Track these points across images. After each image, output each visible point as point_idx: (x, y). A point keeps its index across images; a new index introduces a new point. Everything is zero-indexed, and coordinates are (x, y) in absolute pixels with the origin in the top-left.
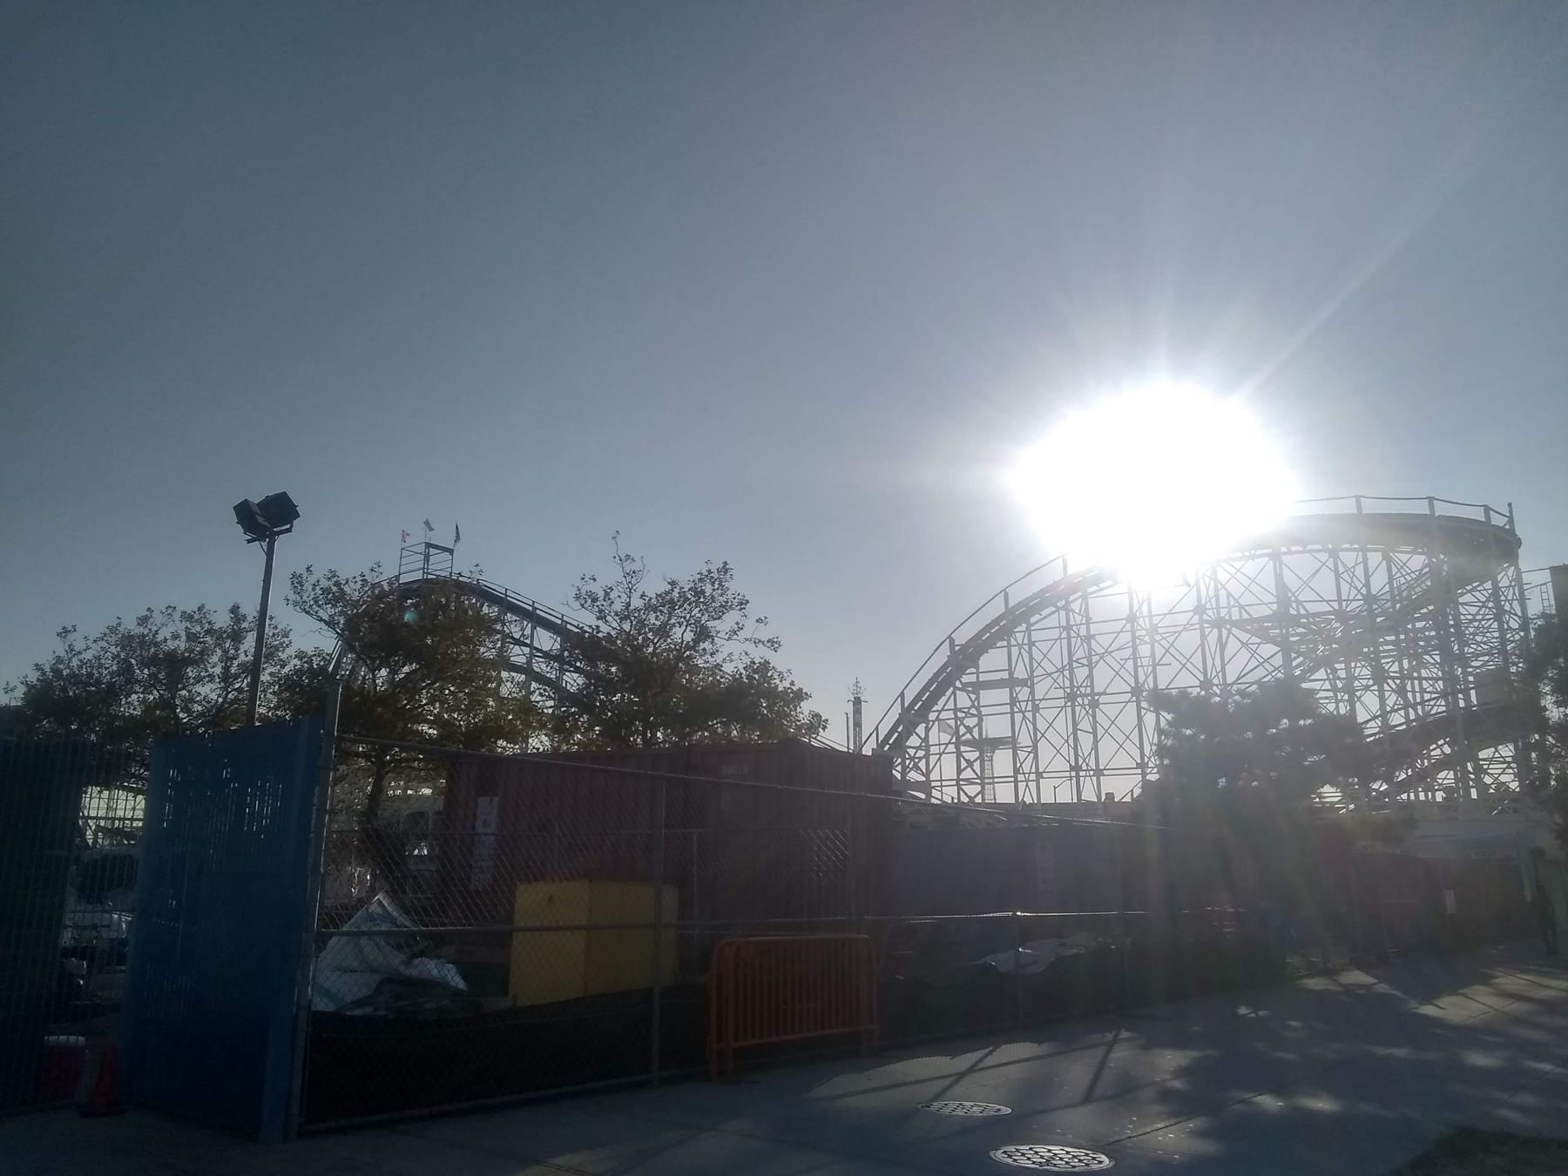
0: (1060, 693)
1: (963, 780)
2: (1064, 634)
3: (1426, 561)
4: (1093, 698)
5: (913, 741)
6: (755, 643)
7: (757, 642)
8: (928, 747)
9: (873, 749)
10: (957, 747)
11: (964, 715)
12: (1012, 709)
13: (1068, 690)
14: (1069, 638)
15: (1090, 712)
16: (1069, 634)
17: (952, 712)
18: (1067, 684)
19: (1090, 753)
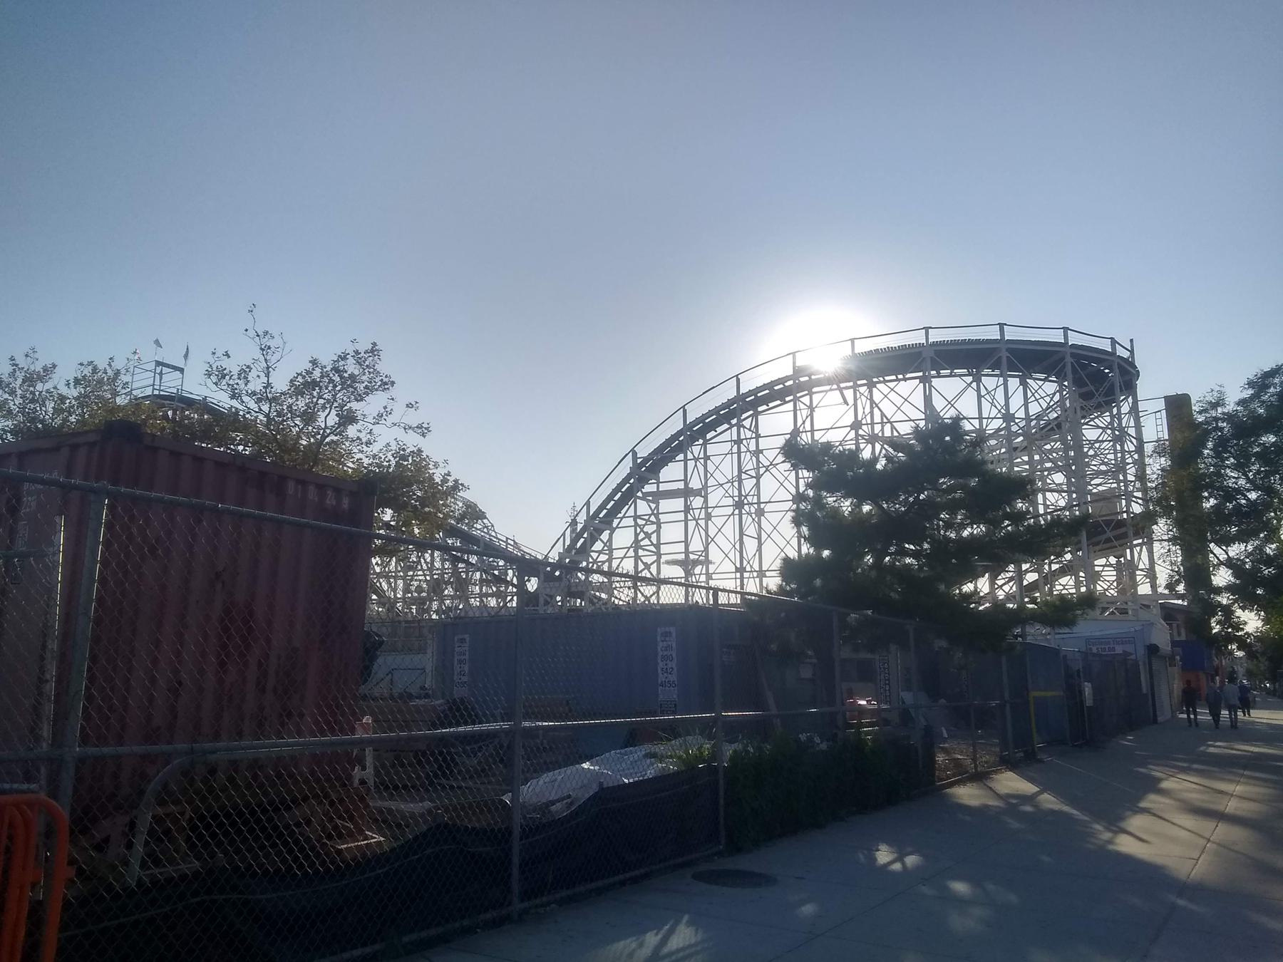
0: (730, 501)
2: (735, 449)
3: (1058, 389)
4: (759, 506)
5: (598, 546)
6: (405, 429)
7: (407, 428)
8: (611, 550)
10: (636, 552)
11: (644, 522)
12: (686, 517)
13: (737, 499)
14: (739, 453)
15: (756, 519)
16: (739, 448)
17: (632, 518)
18: (736, 493)
19: (755, 555)
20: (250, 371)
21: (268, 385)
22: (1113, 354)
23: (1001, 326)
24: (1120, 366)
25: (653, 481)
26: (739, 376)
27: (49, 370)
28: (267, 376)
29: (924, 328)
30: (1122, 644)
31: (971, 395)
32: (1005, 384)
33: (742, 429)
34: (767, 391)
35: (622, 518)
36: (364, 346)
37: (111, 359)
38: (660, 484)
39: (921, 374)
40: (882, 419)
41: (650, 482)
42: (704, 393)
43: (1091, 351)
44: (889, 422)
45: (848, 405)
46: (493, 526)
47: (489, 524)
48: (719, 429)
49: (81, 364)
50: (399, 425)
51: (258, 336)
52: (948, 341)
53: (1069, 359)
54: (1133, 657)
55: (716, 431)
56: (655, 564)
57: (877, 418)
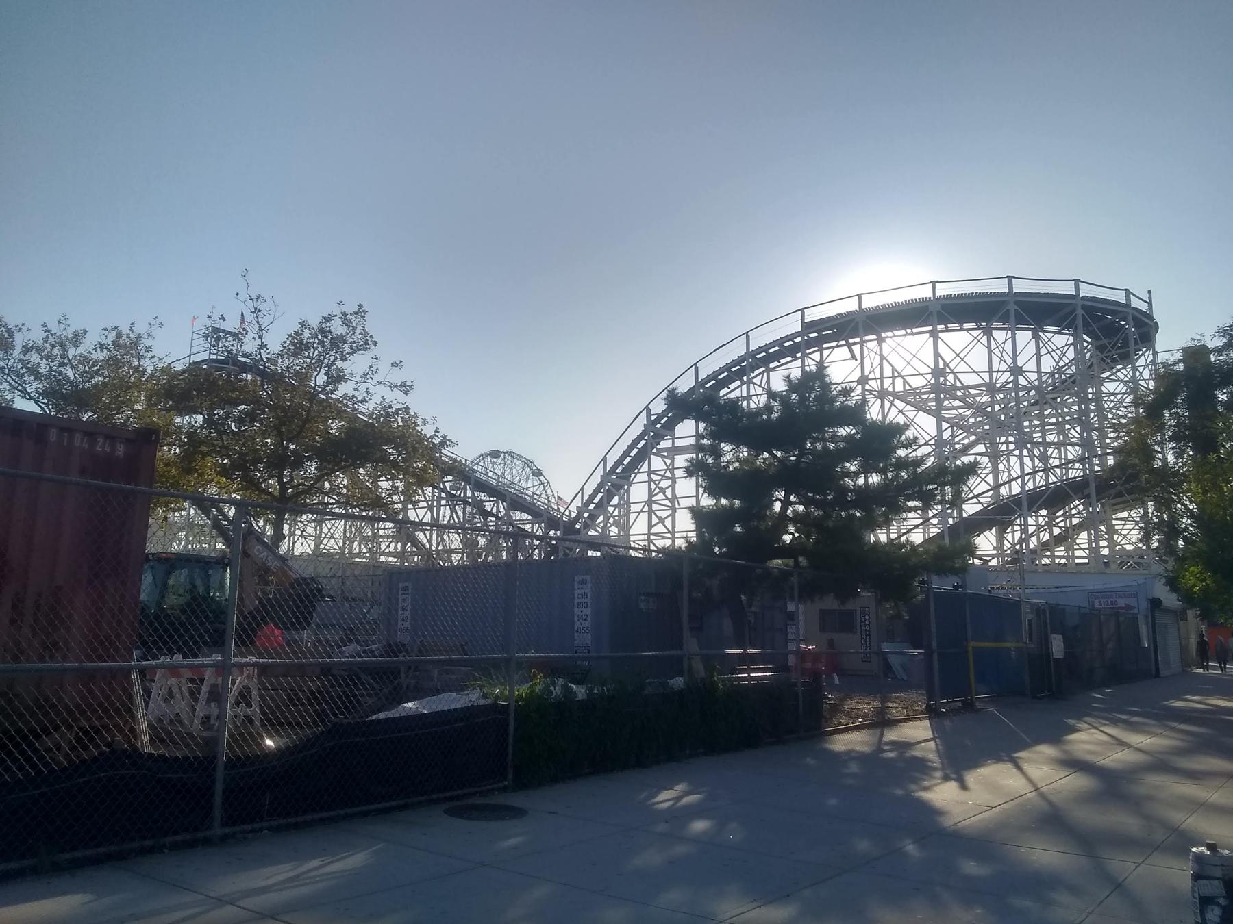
1: (654, 534)
6: (391, 387)
9: (577, 507)
10: (650, 507)
11: (659, 478)
17: (646, 474)
20: (246, 334)
21: (263, 346)
22: (1128, 305)
23: (1010, 278)
24: (1134, 318)
25: (669, 437)
26: (749, 333)
27: (77, 339)
28: (261, 337)
29: (931, 282)
30: (1125, 597)
31: (981, 351)
32: (1013, 338)
33: (751, 385)
34: (777, 348)
35: (636, 474)
36: (351, 308)
37: (132, 324)
38: (676, 440)
39: (931, 328)
40: (893, 373)
41: (666, 438)
42: (715, 351)
43: (1061, 298)
44: (900, 376)
45: (856, 360)
46: (548, 483)
47: (546, 481)
48: (732, 386)
49: (105, 330)
50: (384, 384)
51: (251, 299)
52: (955, 295)
53: (1080, 312)
54: (1135, 611)
55: (729, 388)
56: (670, 518)
57: (888, 372)
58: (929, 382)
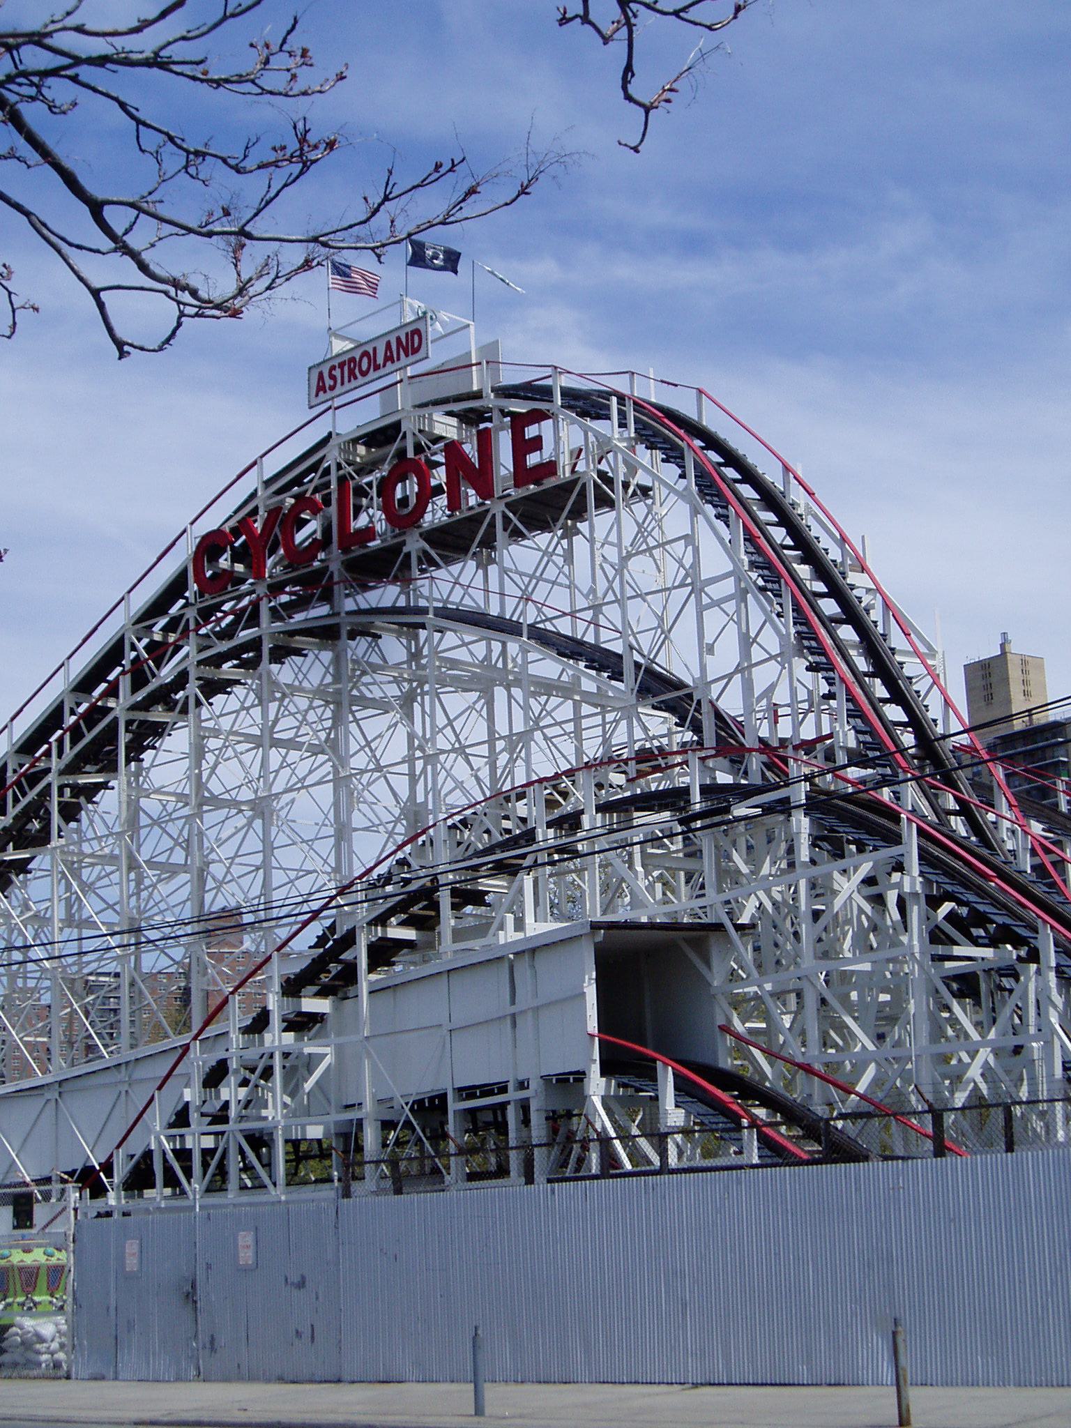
58: (469, 586)
